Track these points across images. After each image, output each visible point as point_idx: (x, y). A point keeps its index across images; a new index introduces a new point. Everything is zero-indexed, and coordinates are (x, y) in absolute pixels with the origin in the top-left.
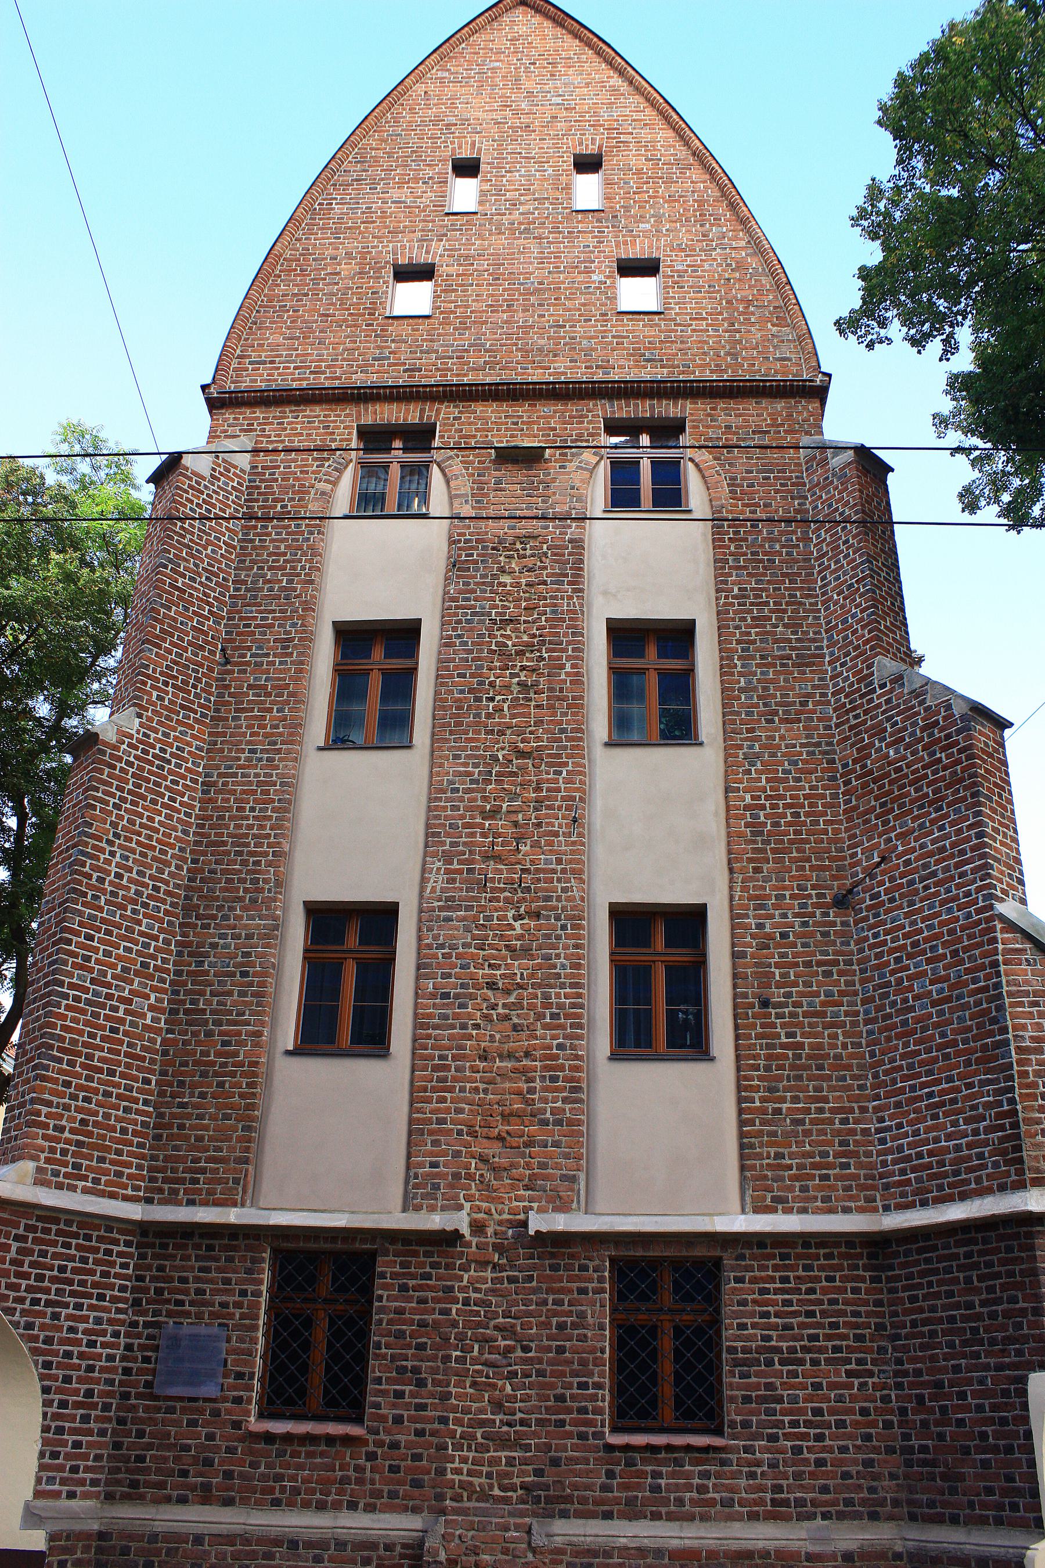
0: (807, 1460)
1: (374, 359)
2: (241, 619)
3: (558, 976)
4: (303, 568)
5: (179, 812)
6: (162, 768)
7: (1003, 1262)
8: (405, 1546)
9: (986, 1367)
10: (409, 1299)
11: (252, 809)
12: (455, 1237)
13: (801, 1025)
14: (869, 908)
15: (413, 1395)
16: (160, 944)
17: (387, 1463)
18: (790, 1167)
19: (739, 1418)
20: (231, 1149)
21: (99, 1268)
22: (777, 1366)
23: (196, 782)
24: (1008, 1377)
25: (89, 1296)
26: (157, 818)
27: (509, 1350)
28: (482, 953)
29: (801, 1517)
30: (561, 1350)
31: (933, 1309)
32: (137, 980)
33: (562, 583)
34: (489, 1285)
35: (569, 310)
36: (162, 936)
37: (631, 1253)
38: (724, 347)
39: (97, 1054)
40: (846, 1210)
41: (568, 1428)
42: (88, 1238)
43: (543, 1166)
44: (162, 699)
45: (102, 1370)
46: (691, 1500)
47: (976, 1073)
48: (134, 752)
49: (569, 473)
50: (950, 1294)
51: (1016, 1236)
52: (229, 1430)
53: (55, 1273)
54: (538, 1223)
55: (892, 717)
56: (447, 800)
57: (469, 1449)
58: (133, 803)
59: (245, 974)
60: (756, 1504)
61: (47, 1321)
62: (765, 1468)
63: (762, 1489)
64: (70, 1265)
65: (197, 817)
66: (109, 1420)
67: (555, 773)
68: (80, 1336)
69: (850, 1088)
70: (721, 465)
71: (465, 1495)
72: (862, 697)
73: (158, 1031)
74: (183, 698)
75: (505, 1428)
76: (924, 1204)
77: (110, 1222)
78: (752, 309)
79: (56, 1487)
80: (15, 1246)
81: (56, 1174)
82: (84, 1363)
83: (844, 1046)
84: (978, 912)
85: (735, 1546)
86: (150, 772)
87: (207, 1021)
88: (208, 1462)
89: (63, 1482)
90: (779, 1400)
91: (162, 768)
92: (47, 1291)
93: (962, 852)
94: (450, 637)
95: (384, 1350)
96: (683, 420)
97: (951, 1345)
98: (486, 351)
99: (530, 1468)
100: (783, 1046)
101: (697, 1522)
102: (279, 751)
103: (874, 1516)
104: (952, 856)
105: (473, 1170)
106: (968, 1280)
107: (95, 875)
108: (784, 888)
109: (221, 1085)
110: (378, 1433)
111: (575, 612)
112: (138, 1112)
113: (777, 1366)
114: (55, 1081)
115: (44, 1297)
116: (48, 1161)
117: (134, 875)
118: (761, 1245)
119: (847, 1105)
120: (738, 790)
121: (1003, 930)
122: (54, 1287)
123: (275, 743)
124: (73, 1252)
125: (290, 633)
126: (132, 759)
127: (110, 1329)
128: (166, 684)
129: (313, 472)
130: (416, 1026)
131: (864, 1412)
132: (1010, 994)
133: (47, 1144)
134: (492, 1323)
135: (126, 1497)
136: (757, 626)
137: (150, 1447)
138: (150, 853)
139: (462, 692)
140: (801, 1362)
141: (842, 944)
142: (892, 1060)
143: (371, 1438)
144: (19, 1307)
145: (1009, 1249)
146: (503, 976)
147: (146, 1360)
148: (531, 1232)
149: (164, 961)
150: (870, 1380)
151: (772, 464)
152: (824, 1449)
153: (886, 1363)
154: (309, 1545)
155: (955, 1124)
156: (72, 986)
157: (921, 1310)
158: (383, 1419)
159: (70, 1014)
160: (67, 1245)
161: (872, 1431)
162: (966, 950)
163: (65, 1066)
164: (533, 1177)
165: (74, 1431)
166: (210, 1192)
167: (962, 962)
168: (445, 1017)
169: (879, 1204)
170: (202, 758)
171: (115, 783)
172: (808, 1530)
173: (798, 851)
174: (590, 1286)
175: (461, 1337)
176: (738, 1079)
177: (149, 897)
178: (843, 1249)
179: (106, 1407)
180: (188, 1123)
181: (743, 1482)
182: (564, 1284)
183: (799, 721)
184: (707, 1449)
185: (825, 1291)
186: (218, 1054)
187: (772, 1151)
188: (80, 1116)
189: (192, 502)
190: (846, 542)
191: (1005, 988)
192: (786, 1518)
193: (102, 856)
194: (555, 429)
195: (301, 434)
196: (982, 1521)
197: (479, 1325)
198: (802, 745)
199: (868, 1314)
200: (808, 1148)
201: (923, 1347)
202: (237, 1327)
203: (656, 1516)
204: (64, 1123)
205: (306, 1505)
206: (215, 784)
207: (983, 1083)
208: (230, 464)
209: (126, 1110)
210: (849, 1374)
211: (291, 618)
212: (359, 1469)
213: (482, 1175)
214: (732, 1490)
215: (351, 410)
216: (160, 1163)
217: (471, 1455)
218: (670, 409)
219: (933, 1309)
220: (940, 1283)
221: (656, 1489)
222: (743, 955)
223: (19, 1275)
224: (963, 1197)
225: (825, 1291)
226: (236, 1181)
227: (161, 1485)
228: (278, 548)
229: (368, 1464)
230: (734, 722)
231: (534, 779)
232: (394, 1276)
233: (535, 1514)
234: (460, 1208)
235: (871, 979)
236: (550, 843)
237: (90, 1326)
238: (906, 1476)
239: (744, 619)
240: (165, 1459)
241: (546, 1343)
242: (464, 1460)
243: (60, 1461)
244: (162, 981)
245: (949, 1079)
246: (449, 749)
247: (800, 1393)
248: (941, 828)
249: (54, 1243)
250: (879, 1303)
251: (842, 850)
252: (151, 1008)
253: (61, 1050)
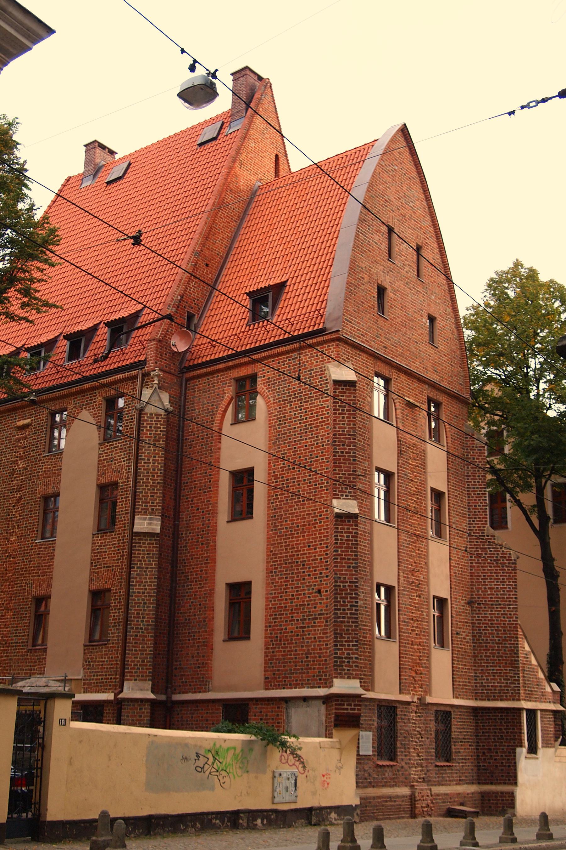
76: (489, 700)
196: (500, 784)
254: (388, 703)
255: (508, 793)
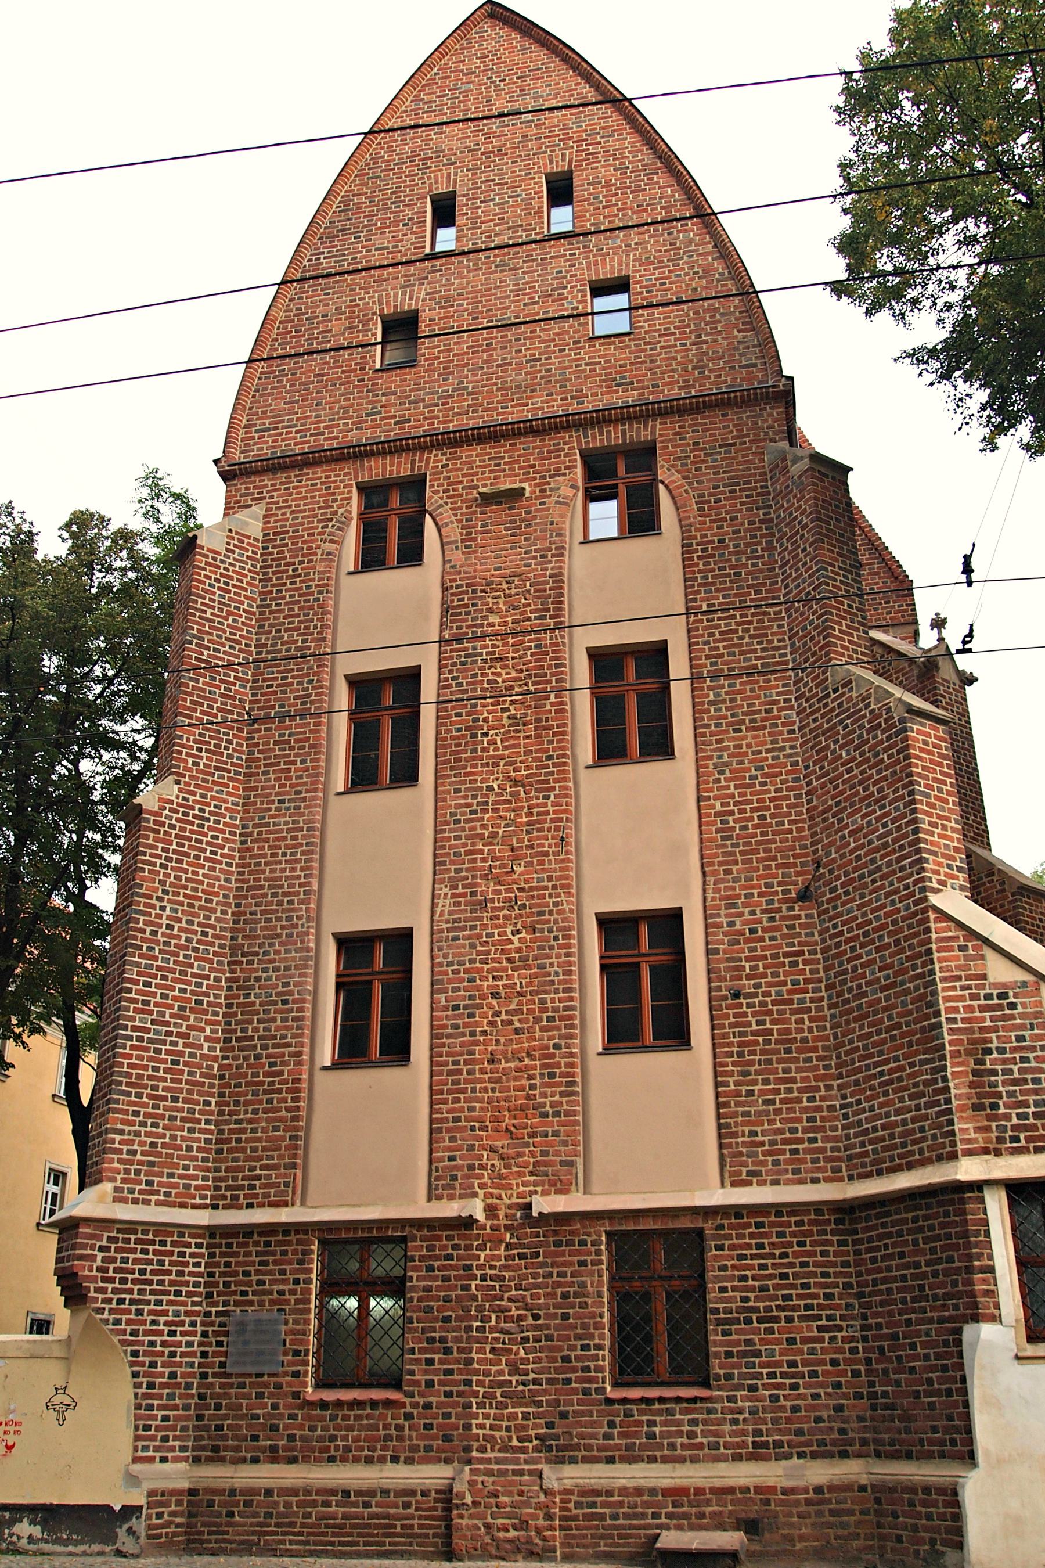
0: (784, 1406)
1: (367, 415)
2: (264, 680)
3: (552, 982)
4: (315, 627)
5: (221, 863)
6: (203, 826)
7: (943, 1226)
8: (437, 1492)
9: (931, 1321)
10: (435, 1278)
11: (284, 854)
12: (469, 1222)
13: (770, 1013)
14: (829, 901)
15: (441, 1362)
16: (211, 982)
17: (422, 1422)
18: (763, 1144)
19: (722, 1372)
20: (281, 1157)
21: (174, 1269)
22: (755, 1324)
23: (234, 834)
24: (947, 1329)
25: (168, 1293)
26: (201, 872)
27: (520, 1318)
28: (486, 967)
29: (779, 1458)
30: (565, 1317)
31: (889, 1269)
32: (193, 1016)
33: (544, 618)
34: (503, 1262)
35: (544, 341)
36: (212, 975)
37: (624, 1228)
38: (692, 361)
39: (161, 1084)
40: (815, 1181)
41: (574, 1385)
42: (163, 1243)
43: (545, 1153)
44: (198, 764)
45: (183, 1355)
46: (682, 1445)
47: (917, 1053)
48: (175, 816)
49: (548, 509)
50: (902, 1255)
51: (952, 1202)
52: (290, 1400)
53: (137, 1276)
54: (543, 1204)
55: (843, 720)
56: (451, 831)
57: (491, 1407)
58: (178, 861)
59: (285, 1002)
60: (739, 1447)
61: (132, 1317)
62: (747, 1415)
63: (744, 1433)
64: (149, 1268)
65: (237, 865)
66: (192, 1396)
67: (544, 797)
68: (161, 1327)
69: (816, 1068)
70: (690, 484)
71: (489, 1446)
72: (819, 701)
73: (215, 1059)
74: (217, 761)
75: (521, 1388)
77: (181, 1229)
78: (718, 317)
79: (151, 1454)
80: (100, 1256)
81: (132, 1191)
82: (167, 1351)
83: (810, 1030)
84: (916, 904)
85: (718, 1483)
86: (192, 831)
87: (255, 1046)
88: (274, 1428)
89: (156, 1449)
90: (758, 1354)
91: (202, 826)
92: (130, 1291)
93: (902, 848)
94: (446, 679)
95: (415, 1324)
96: (654, 442)
97: (904, 1301)
98: (469, 394)
99: (542, 1421)
100: (754, 1033)
101: (688, 1463)
102: (304, 799)
103: (844, 1455)
104: (894, 851)
105: (485, 1161)
106: (915, 1242)
107: (148, 929)
108: (753, 887)
109: (270, 1101)
110: (413, 1396)
111: (557, 644)
112: (201, 1131)
113: (755, 1324)
114: (126, 1112)
115: (128, 1297)
116: (124, 1181)
117: (184, 925)
118: (738, 1215)
119: (813, 1084)
120: (709, 798)
121: (936, 920)
122: (136, 1288)
123: (300, 792)
124: (151, 1256)
125: (307, 689)
126: (174, 822)
127: (187, 1319)
128: (200, 750)
129: (319, 534)
130: (432, 1036)
131: (834, 1363)
132: (944, 980)
133: (122, 1167)
134: (506, 1295)
135: (210, 1460)
136: (724, 640)
137: (226, 1417)
138: (197, 903)
139: (459, 730)
140: (776, 1319)
141: (807, 935)
142: (851, 1042)
143: (407, 1400)
144: (107, 1306)
145: (946, 1214)
146: (505, 986)
147: (219, 1344)
148: (535, 1214)
149: (216, 996)
150: (839, 1335)
151: (738, 477)
152: (799, 1397)
153: (853, 1318)
154: (359, 1493)
155: (901, 1100)
156: (135, 1029)
157: (879, 1270)
158: (417, 1383)
159: (135, 1053)
160: (145, 1252)
161: (842, 1379)
162: (906, 938)
163: (133, 1099)
164: (536, 1164)
165: (161, 1407)
166: (266, 1195)
167: (902, 951)
168: (457, 1027)
169: (845, 1173)
170: (238, 812)
171: (160, 845)
172: (784, 1469)
173: (765, 851)
174: (589, 1258)
175: (480, 1309)
176: (715, 1065)
177: (199, 942)
178: (813, 1217)
179: (189, 1386)
180: (244, 1137)
181: (727, 1428)
182: (567, 1258)
183: (764, 727)
184: (694, 1400)
185: (796, 1255)
186: (267, 1074)
187: (747, 1129)
188: (149, 1140)
189: (210, 578)
190: (804, 550)
191: (938, 974)
192: (765, 1458)
193: (153, 912)
194: (534, 466)
195: (306, 498)
196: (929, 1456)
197: (495, 1298)
198: (768, 751)
199: (836, 1275)
200: (779, 1125)
201: (882, 1304)
202: (293, 1312)
203: (652, 1460)
204: (135, 1147)
205: (356, 1460)
206: (251, 834)
207: (923, 1062)
208: (243, 535)
209: (190, 1130)
210: (820, 1329)
211: (308, 675)
212: (399, 1428)
213: (493, 1165)
214: (717, 1434)
215: (349, 467)
216: (223, 1174)
217: (492, 1412)
218: (639, 433)
219: (889, 1269)
220: (895, 1245)
221: (651, 1436)
222: (716, 951)
223: (105, 1280)
224: (910, 1167)
225: (796, 1255)
226: (286, 1184)
227: (238, 1449)
228: (292, 610)
229: (407, 1424)
230: (704, 735)
231: (525, 804)
232: (422, 1258)
233: (548, 1461)
234: (475, 1195)
235: (833, 966)
236: (542, 863)
237: (170, 1318)
238: (872, 1419)
239: (712, 635)
240: (240, 1427)
241: (552, 1311)
242: (486, 1416)
243: (152, 1432)
244: (217, 1014)
245: (896, 1059)
246: (451, 784)
247: (777, 1348)
248: (884, 826)
249: (134, 1251)
250: (845, 1264)
251: (805, 847)
252: (207, 1039)
253: (128, 1084)
254: (379, 1229)
255: (941, 1491)
